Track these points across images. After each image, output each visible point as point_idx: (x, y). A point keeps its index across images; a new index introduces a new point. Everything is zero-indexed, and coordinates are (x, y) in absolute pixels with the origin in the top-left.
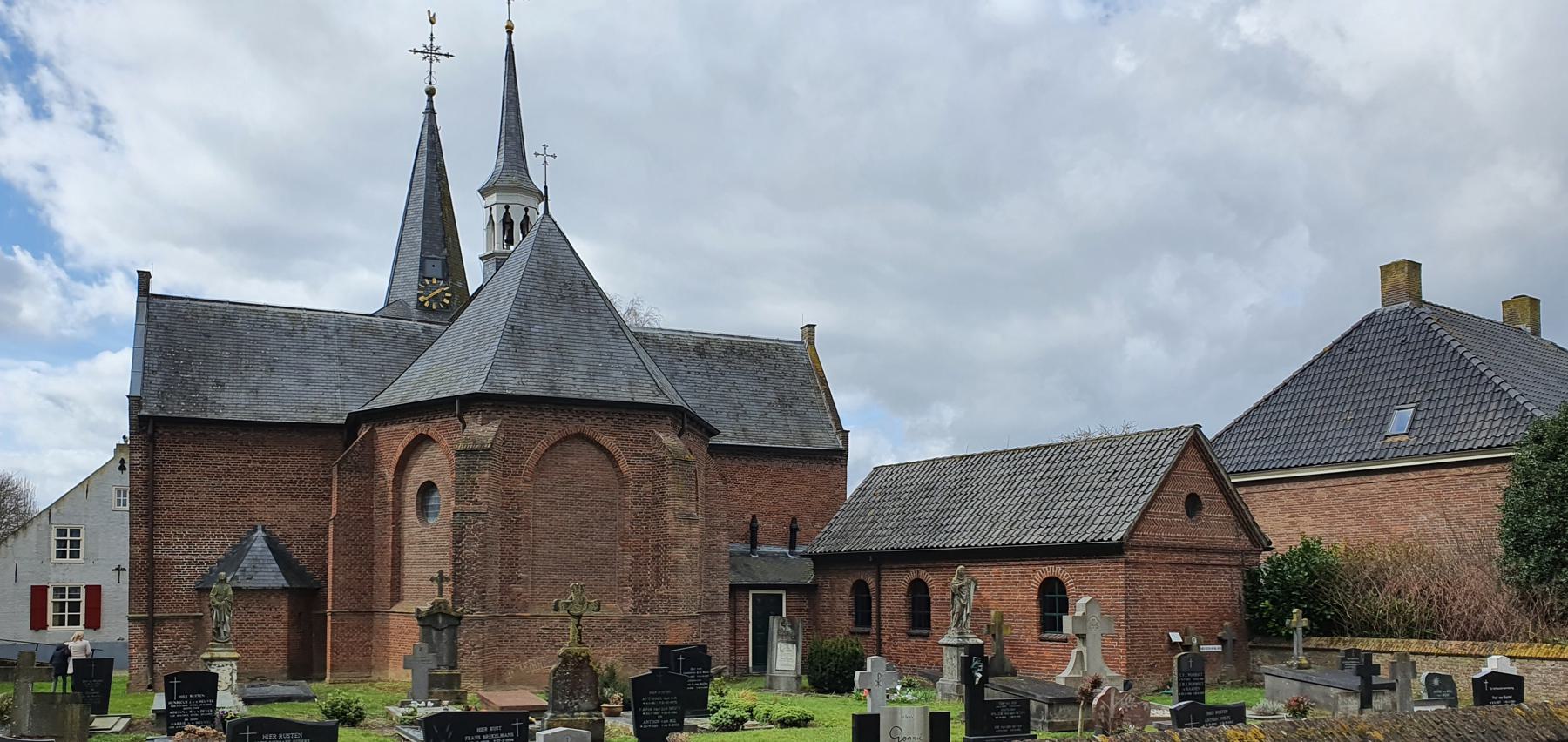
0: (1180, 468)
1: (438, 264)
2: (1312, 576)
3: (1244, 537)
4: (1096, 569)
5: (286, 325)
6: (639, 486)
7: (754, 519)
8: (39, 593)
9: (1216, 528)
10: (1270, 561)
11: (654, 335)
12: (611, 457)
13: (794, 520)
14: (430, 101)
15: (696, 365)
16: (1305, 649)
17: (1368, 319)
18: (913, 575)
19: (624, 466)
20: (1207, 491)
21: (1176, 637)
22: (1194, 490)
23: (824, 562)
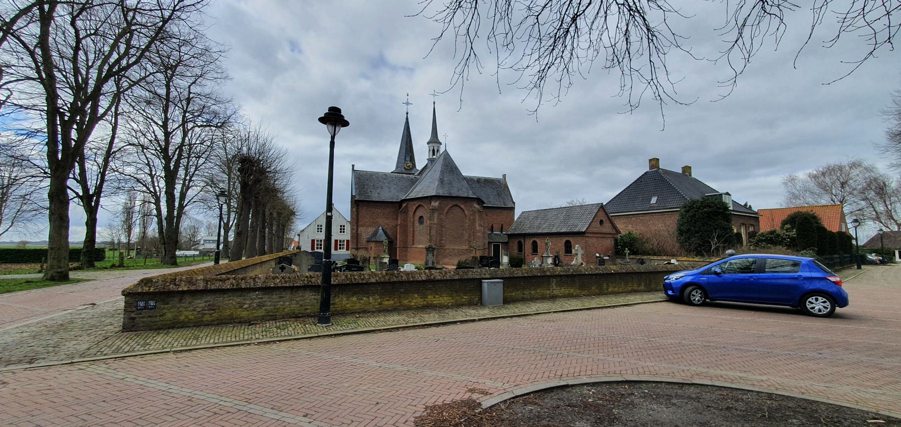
0: (598, 214)
1: (409, 157)
2: (631, 241)
3: (614, 230)
4: (579, 239)
5: (384, 177)
6: (469, 217)
7: (492, 225)
8: (313, 241)
9: (607, 228)
10: (620, 236)
11: (467, 178)
12: (463, 210)
13: (502, 225)
14: (407, 116)
15: (478, 185)
16: (629, 259)
17: (646, 173)
18: (533, 239)
19: (466, 212)
20: (605, 219)
21: (598, 255)
22: (602, 219)
23: (511, 236)
